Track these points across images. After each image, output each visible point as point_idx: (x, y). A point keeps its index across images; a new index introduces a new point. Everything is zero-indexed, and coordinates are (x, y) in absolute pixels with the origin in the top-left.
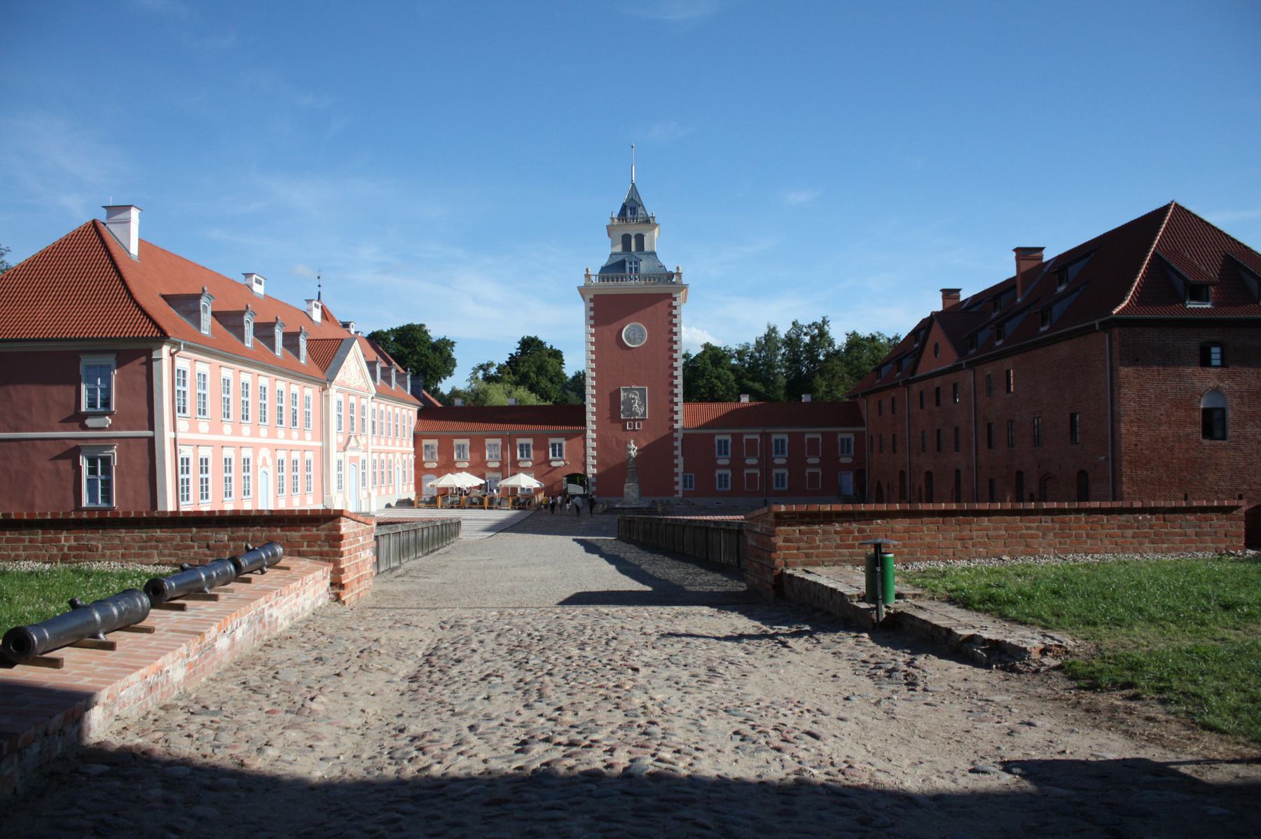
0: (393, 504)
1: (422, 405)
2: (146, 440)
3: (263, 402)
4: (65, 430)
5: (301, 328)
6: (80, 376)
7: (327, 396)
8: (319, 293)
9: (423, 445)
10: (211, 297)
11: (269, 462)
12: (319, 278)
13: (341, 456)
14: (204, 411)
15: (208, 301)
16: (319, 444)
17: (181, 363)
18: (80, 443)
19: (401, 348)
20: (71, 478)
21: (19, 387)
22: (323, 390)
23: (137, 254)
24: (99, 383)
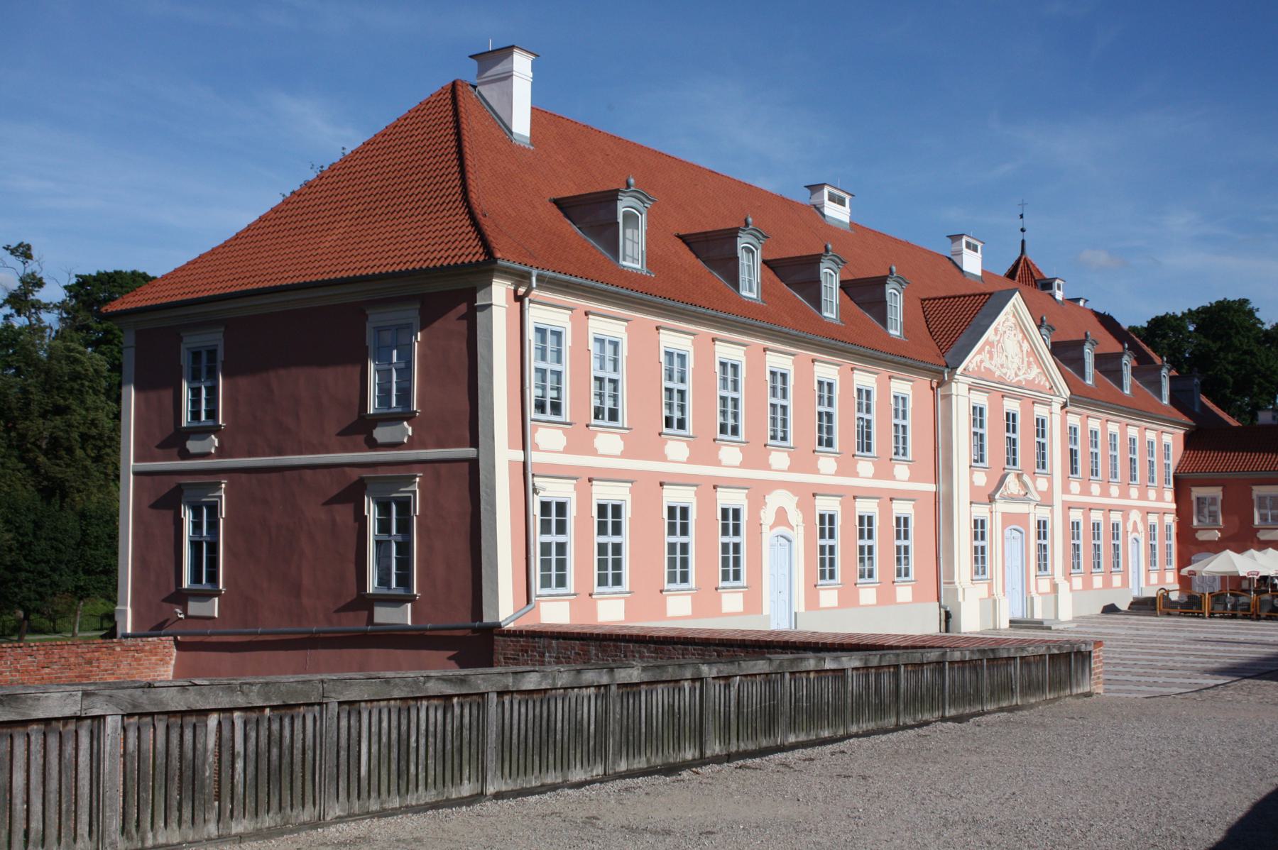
0: (1124, 606)
1: (1192, 423)
2: (466, 464)
3: (1094, 450)
4: (346, 450)
5: (1086, 334)
6: (367, 347)
7: (948, 397)
8: (1023, 242)
9: (1194, 498)
10: (901, 281)
11: (1140, 527)
12: (1022, 216)
13: (981, 511)
14: (1014, 460)
15: (898, 287)
17: (537, 315)
18: (366, 474)
19: (1204, 341)
20: (352, 541)
21: (282, 372)
22: (939, 385)
23: (528, 134)
24: (395, 360)
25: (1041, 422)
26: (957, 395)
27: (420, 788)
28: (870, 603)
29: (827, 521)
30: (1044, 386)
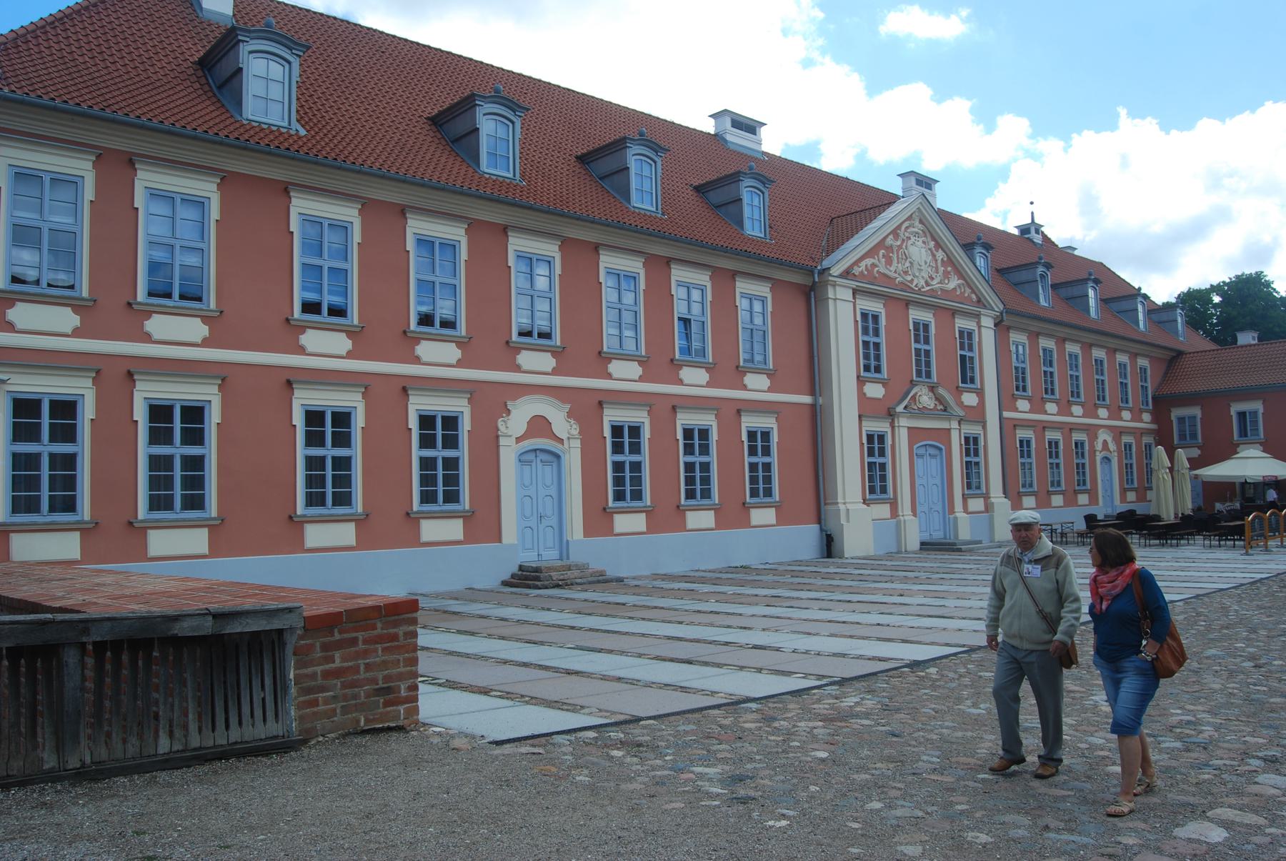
16: (807, 399)
25: (967, 336)
26: (835, 300)
27: (257, 722)
28: (886, 517)
29: (625, 437)
30: (969, 297)
